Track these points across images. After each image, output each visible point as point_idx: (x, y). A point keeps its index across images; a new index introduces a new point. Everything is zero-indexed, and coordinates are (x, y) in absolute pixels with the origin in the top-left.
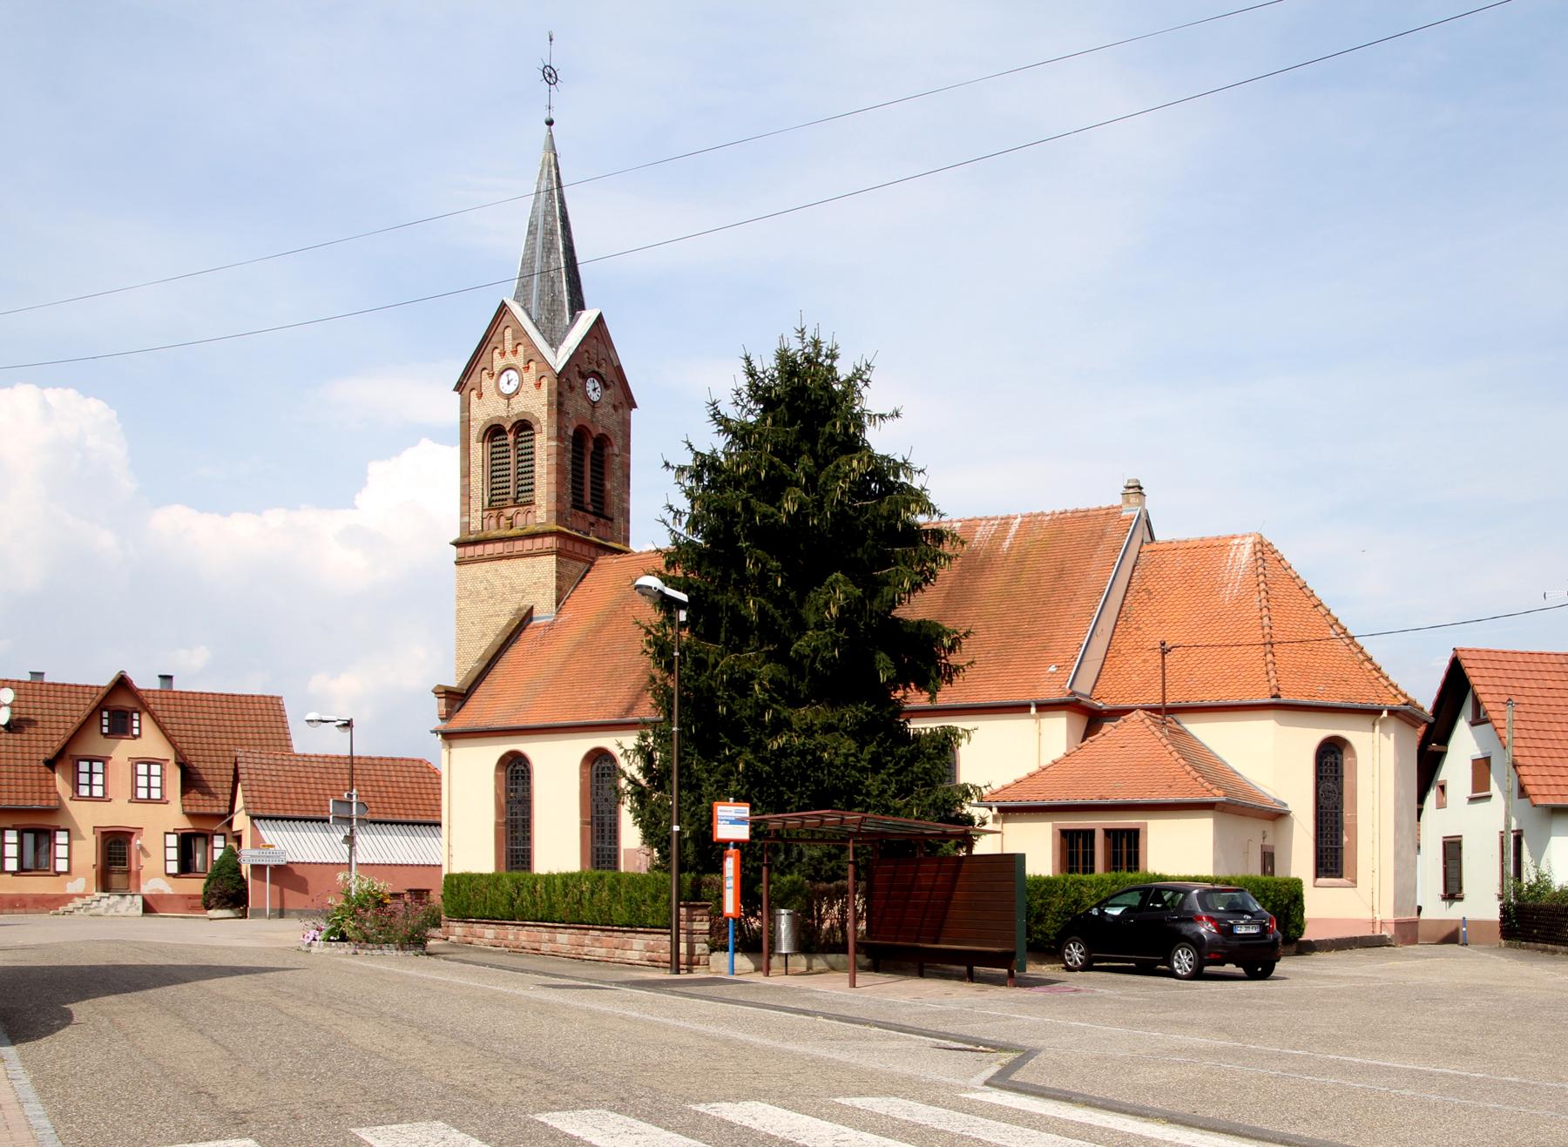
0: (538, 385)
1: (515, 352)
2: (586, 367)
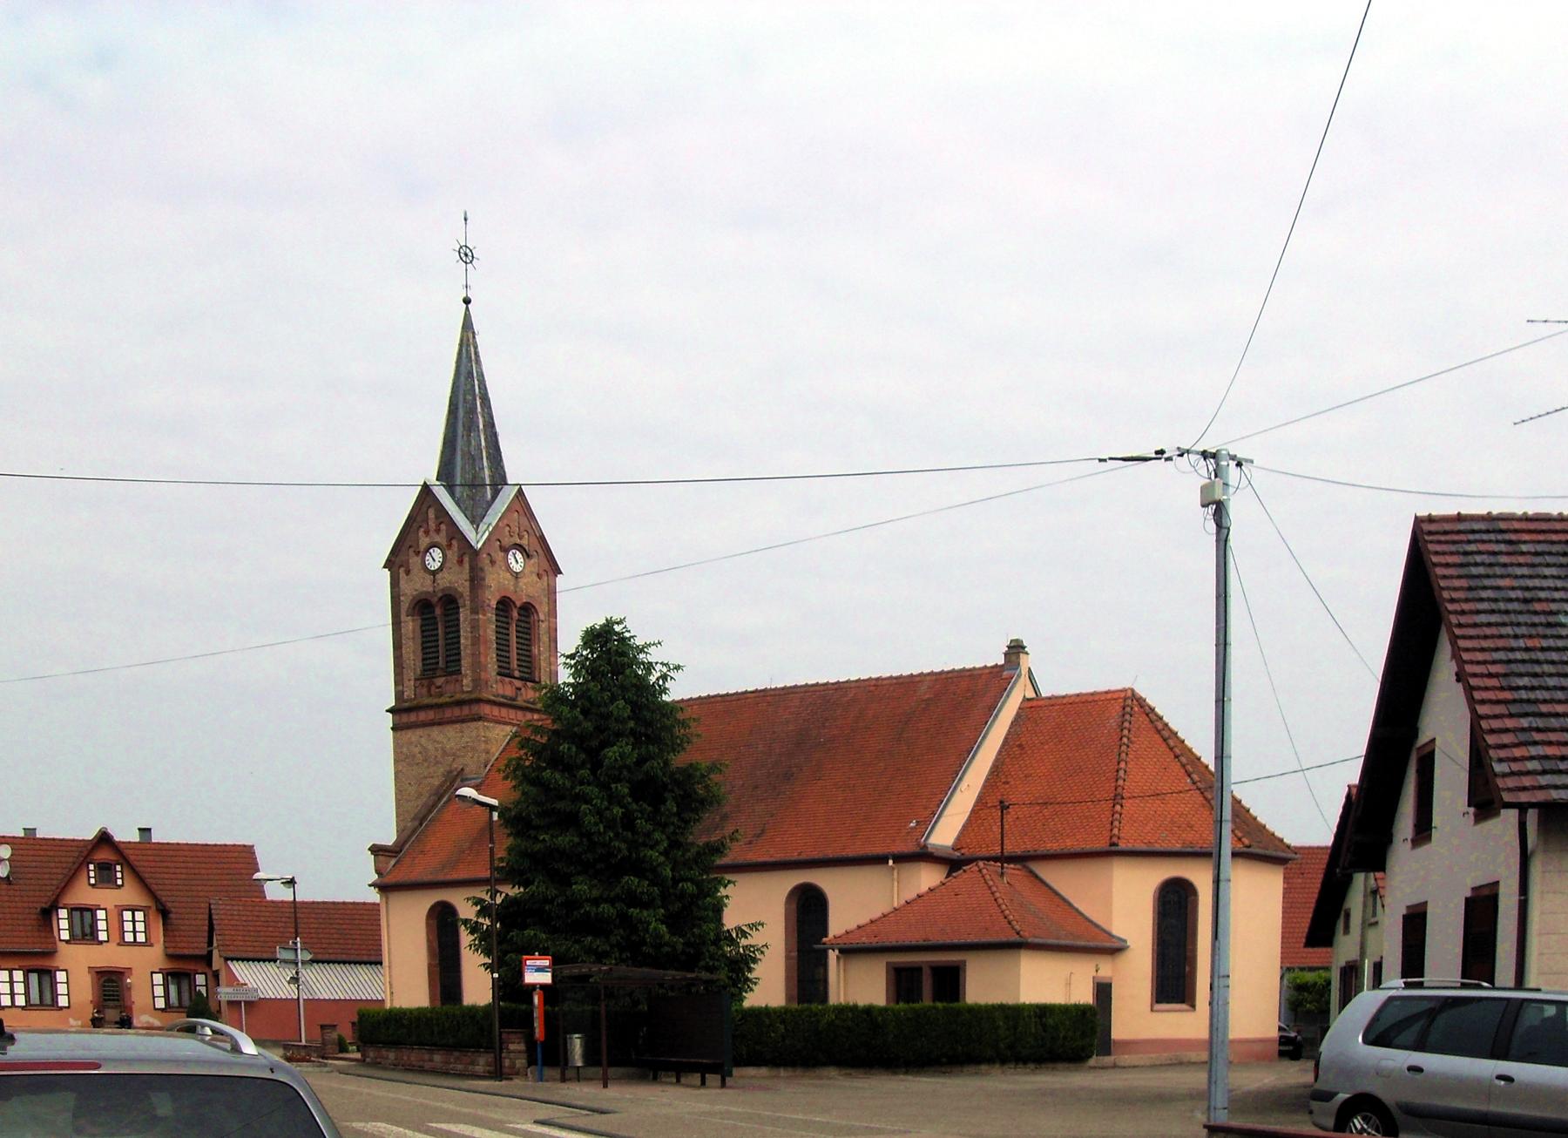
0: (460, 562)
1: (438, 531)
2: (507, 541)
